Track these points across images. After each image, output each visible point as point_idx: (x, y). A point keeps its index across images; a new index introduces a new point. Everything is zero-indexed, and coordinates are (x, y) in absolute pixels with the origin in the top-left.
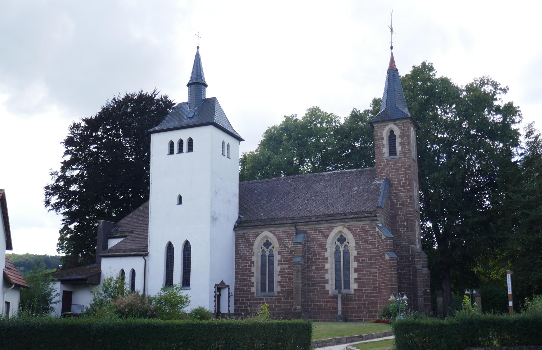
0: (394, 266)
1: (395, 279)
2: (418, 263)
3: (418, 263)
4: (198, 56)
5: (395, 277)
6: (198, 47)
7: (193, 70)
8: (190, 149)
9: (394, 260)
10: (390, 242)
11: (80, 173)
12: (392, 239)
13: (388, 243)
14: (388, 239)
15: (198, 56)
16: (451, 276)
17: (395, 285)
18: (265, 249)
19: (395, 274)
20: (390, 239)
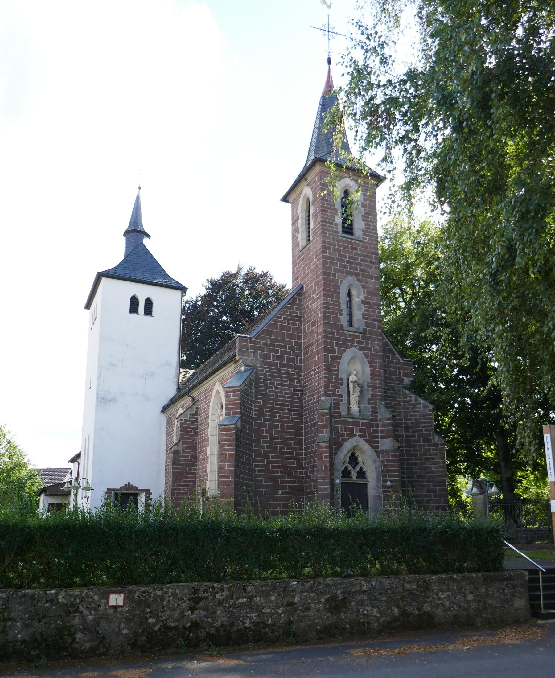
0: (228, 440)
1: (229, 466)
2: (325, 431)
3: (325, 431)
4: (138, 198)
5: (229, 461)
6: (140, 188)
7: (133, 213)
8: (127, 258)
9: (228, 429)
10: (234, 396)
11: (225, 652)
12: (238, 391)
13: (231, 397)
14: (231, 392)
15: (138, 198)
16: (519, 474)
17: (228, 477)
18: (350, 468)
19: (231, 455)
20: (234, 391)
